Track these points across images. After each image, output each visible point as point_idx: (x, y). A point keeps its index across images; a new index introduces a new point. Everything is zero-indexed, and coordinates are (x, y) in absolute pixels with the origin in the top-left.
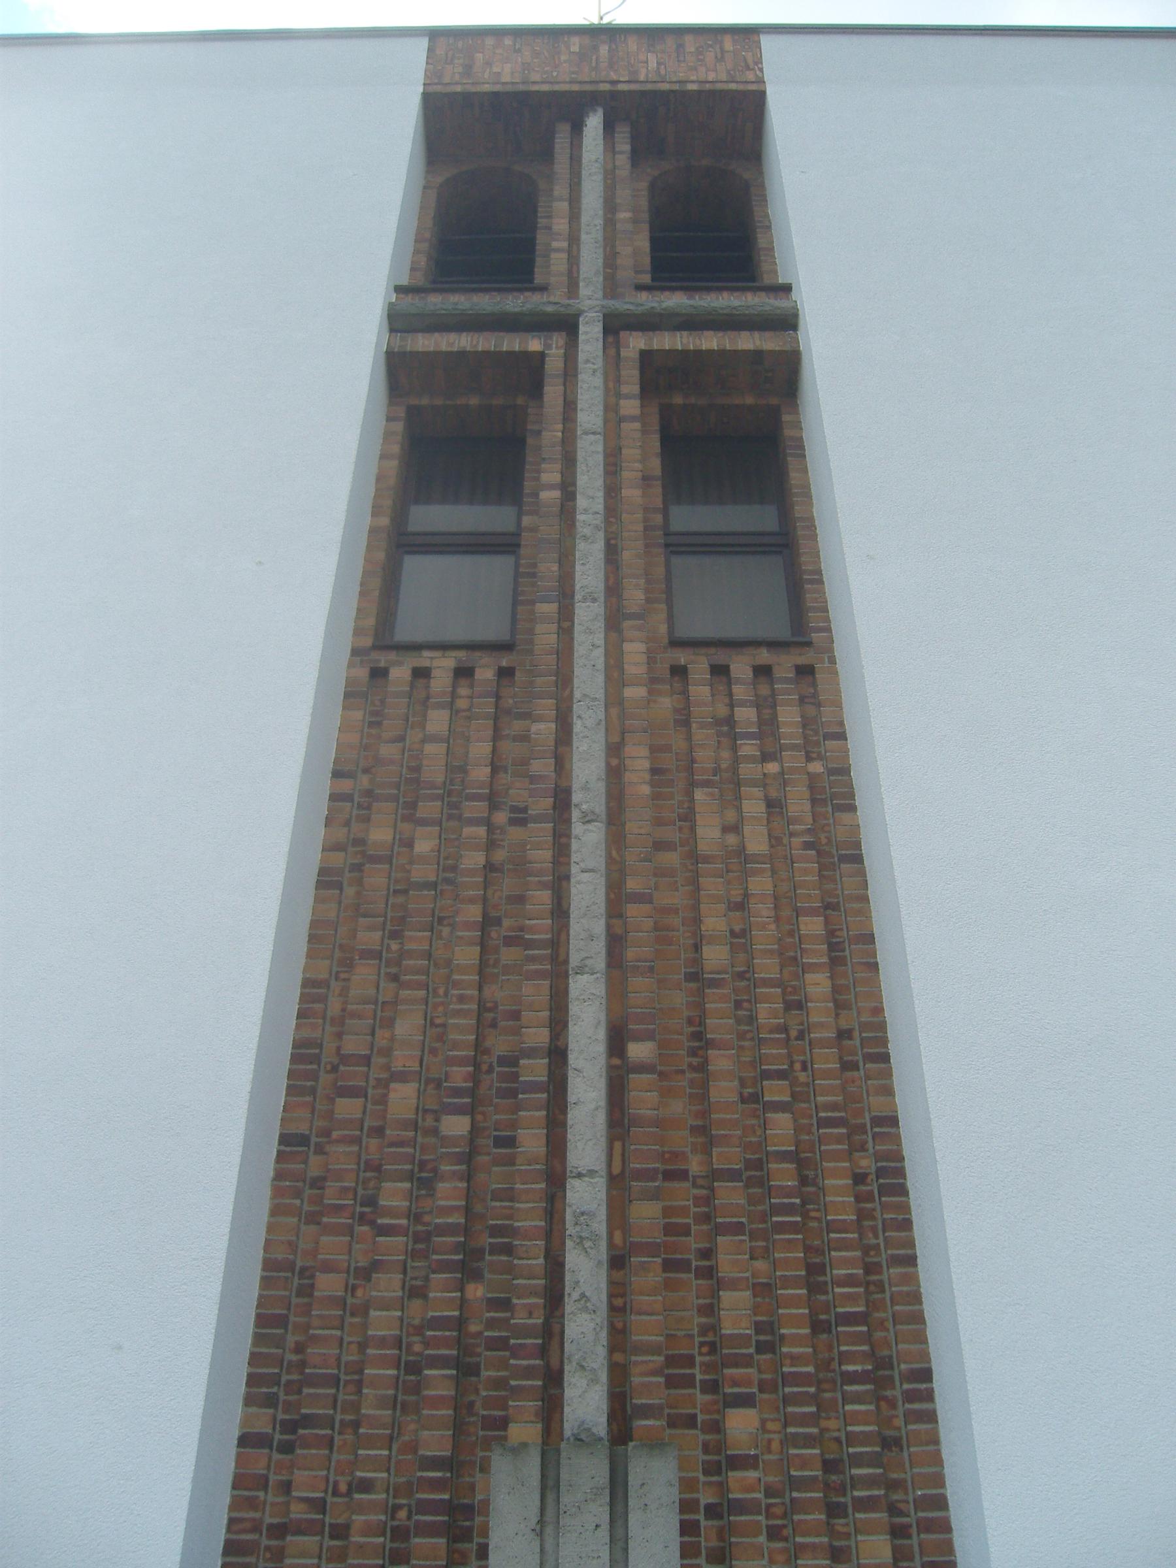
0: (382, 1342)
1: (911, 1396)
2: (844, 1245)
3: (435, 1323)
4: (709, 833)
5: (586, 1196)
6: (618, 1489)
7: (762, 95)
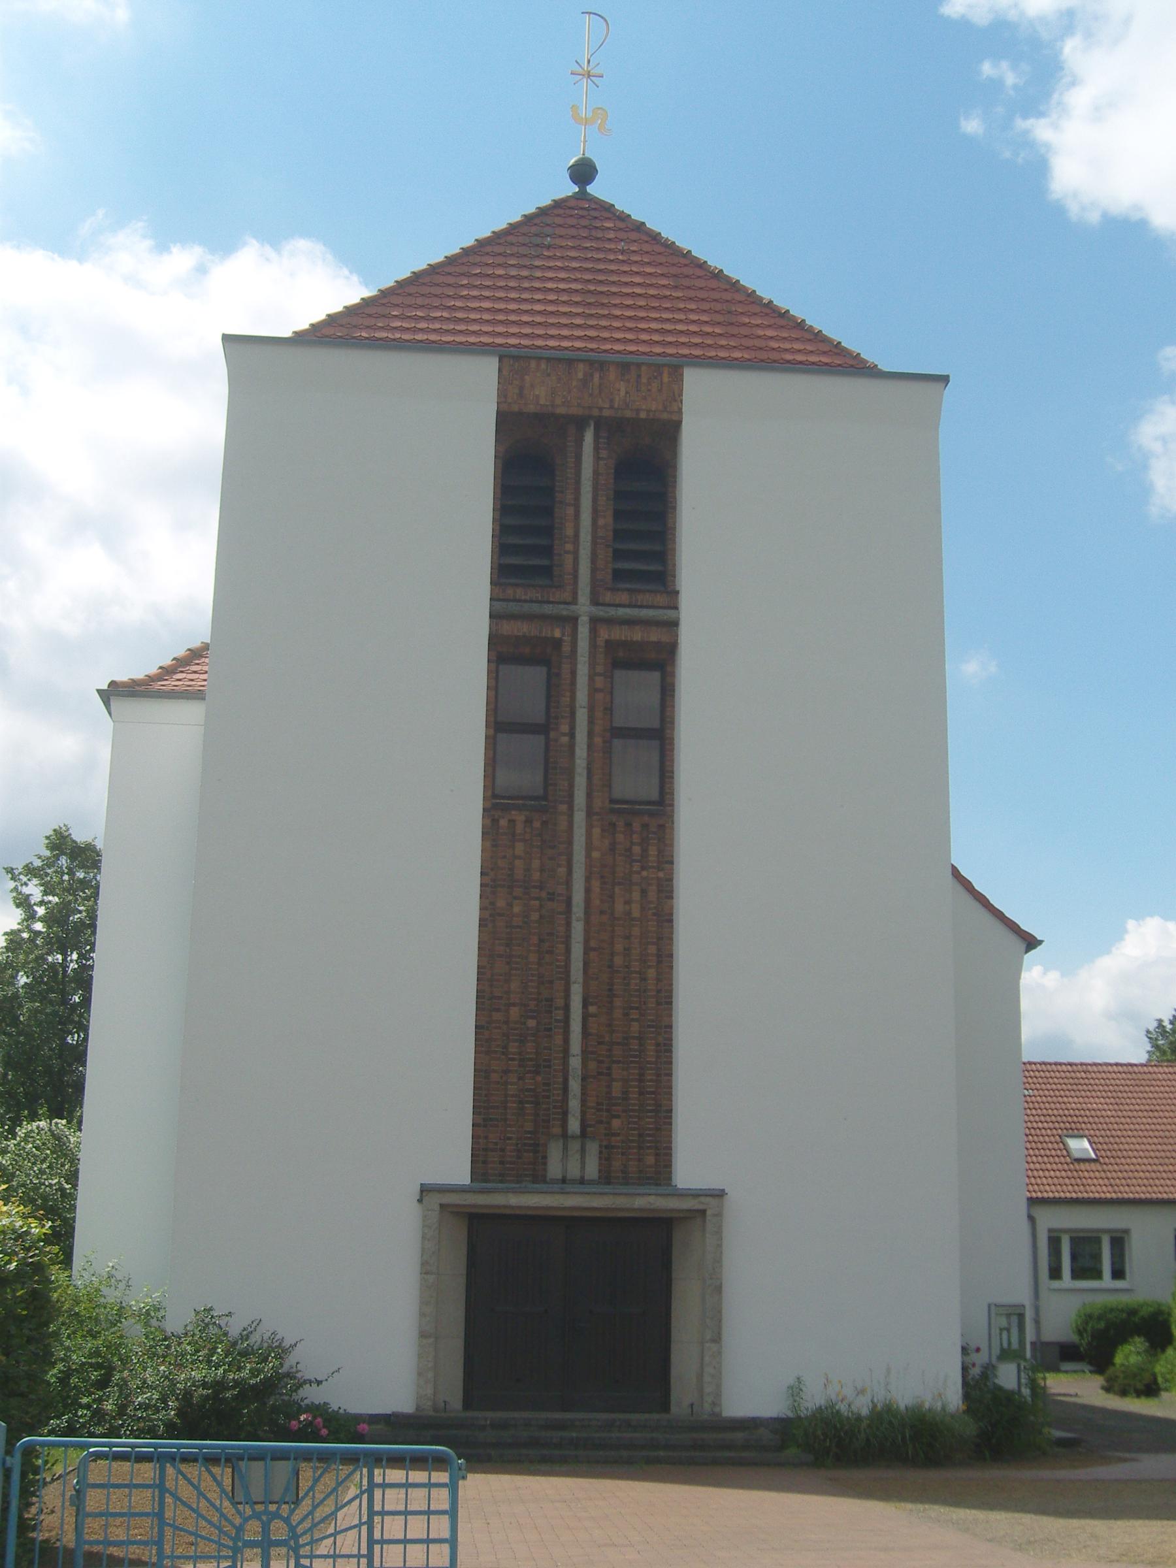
0: (512, 1096)
1: (665, 1117)
2: (651, 1069)
3: (527, 1090)
4: (619, 907)
5: (575, 1062)
6: (583, 1151)
7: (677, 425)
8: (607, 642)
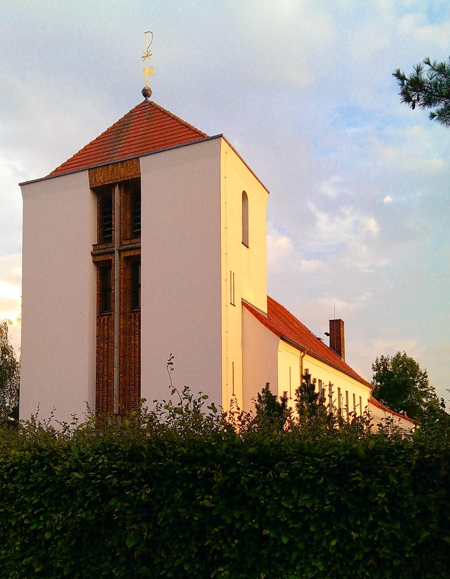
7: (139, 179)
8: (124, 257)
